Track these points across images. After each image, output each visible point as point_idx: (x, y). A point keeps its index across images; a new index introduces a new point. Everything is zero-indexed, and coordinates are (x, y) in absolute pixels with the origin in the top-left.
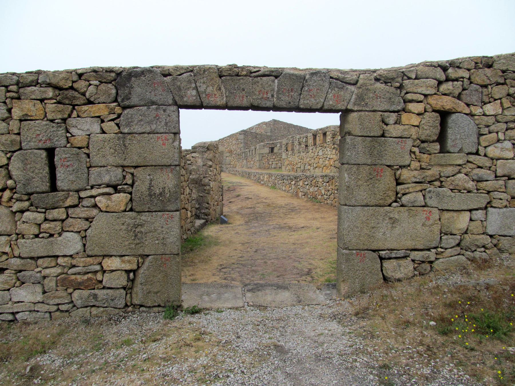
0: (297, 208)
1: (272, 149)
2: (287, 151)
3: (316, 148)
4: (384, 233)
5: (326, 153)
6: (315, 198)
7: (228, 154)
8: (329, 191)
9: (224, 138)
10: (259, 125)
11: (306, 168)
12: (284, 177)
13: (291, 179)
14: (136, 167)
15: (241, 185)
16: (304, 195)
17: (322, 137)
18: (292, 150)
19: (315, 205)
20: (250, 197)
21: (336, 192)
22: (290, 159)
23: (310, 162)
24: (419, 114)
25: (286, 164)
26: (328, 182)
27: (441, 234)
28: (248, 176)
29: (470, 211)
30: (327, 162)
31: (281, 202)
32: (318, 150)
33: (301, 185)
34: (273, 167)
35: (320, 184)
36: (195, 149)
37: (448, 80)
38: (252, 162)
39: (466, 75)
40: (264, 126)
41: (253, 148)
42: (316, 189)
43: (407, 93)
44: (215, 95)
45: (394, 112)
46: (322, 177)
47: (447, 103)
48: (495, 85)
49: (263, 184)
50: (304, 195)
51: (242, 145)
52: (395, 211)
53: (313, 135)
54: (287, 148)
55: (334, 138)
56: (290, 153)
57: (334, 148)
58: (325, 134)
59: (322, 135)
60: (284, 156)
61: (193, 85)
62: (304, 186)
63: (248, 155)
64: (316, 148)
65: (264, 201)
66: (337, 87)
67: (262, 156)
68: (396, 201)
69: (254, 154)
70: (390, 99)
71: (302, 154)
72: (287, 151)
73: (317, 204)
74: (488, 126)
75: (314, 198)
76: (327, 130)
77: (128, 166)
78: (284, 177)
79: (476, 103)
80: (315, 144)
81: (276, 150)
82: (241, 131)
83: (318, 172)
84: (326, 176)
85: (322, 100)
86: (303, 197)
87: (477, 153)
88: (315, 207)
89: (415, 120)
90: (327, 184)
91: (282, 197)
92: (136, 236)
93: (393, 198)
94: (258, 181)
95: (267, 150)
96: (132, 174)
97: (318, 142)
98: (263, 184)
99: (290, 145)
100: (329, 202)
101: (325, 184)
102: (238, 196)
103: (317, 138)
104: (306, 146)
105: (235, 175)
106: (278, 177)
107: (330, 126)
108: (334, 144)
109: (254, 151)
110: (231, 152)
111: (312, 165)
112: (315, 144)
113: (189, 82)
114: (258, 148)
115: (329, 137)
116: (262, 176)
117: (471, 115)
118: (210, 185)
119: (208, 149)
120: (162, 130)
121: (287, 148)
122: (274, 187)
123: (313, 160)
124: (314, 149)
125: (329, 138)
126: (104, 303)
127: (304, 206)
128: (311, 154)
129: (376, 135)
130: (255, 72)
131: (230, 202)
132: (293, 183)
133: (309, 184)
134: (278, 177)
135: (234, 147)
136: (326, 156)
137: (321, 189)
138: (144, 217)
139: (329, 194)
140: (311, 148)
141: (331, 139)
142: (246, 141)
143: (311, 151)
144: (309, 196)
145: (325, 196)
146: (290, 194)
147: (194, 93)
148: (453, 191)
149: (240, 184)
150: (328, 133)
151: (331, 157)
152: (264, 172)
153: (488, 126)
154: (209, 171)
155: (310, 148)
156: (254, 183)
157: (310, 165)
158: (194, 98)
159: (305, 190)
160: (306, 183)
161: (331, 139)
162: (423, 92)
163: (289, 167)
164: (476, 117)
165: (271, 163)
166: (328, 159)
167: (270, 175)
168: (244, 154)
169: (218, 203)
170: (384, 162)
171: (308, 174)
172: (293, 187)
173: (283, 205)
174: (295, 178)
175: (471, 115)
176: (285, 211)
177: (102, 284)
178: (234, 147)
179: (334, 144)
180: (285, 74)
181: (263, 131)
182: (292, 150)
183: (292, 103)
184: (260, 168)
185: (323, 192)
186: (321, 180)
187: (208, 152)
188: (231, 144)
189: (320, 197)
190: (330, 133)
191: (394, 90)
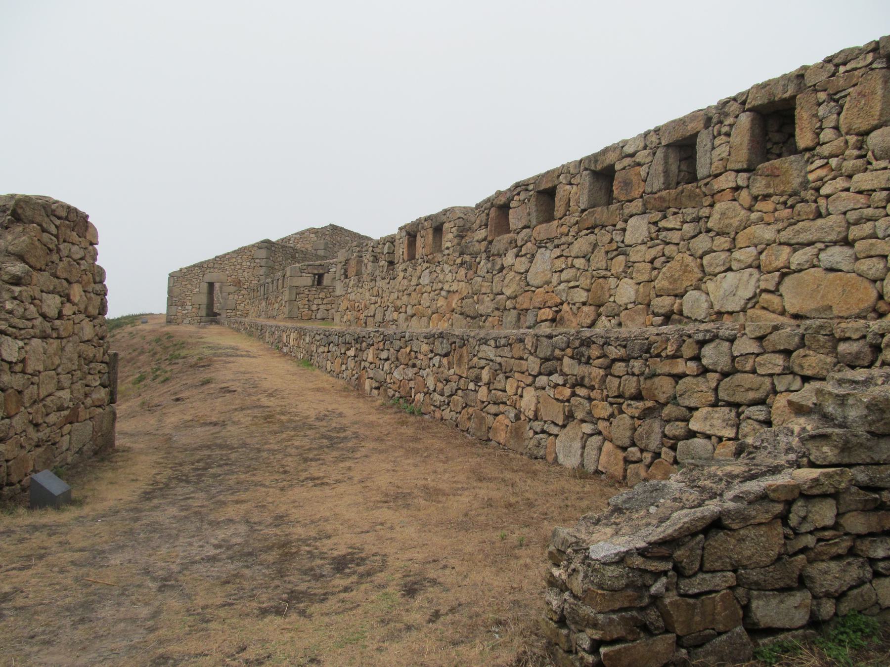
0: (348, 433)
1: (319, 279)
2: (346, 277)
3: (414, 267)
5: (441, 277)
6: (407, 398)
7: (232, 289)
8: (448, 381)
9: (225, 255)
10: (302, 233)
11: (387, 318)
12: (331, 338)
13: (345, 343)
15: (235, 353)
16: (378, 388)
17: (431, 237)
19: (403, 423)
20: (233, 388)
21: (472, 386)
22: (352, 296)
23: (399, 303)
25: (342, 307)
26: (446, 355)
28: (257, 332)
30: (441, 302)
31: (309, 406)
32: (418, 272)
33: (370, 358)
34: (318, 317)
35: (422, 360)
36: (203, 291)
38: (276, 306)
40: (312, 235)
41: (279, 274)
42: (410, 372)
46: (430, 338)
49: (285, 354)
50: (378, 388)
51: (262, 271)
54: (346, 271)
55: (462, 237)
56: (352, 282)
57: (462, 264)
58: (438, 230)
59: (430, 231)
62: (378, 362)
63: (271, 290)
64: (414, 267)
65: (265, 401)
67: (297, 291)
69: (280, 288)
71: (381, 283)
72: (346, 277)
73: (412, 419)
75: (402, 402)
76: (444, 218)
78: (331, 338)
80: (412, 257)
81: (326, 281)
82: (262, 242)
83: (417, 327)
84: (441, 335)
86: (375, 392)
88: (404, 429)
90: (445, 361)
91: (318, 390)
94: (278, 347)
95: (307, 280)
97: (420, 251)
98: (285, 354)
99: (353, 263)
100: (447, 414)
101: (436, 360)
102: (207, 382)
103: (419, 241)
104: (391, 263)
105: (238, 330)
106: (318, 337)
107: (453, 208)
108: (462, 253)
109: (280, 281)
110: (238, 283)
111: (403, 310)
112: (412, 257)
114: (288, 274)
115: (451, 236)
116: (284, 335)
119: (17, 217)
121: (346, 271)
122: (308, 361)
123: (405, 298)
124: (410, 270)
125: (449, 239)
127: (371, 425)
128: (401, 282)
131: (178, 400)
132: (351, 353)
133: (393, 358)
134: (318, 337)
135: (245, 274)
136: (440, 285)
137: (424, 373)
139: (447, 392)
141: (456, 241)
142: (271, 263)
143: (401, 274)
144: (391, 392)
145: (436, 397)
146: (341, 382)
149: (230, 351)
150: (446, 226)
151: (454, 287)
152: (289, 324)
154: (6, 296)
155: (400, 267)
156: (268, 350)
157: (397, 309)
159: (381, 375)
160: (384, 355)
161: (456, 241)
163: (349, 316)
165: (314, 307)
166: (443, 293)
167: (302, 333)
168: (262, 288)
171: (390, 330)
172: (351, 364)
173: (310, 421)
174: (356, 340)
176: (306, 443)
178: (245, 274)
179: (462, 253)
181: (309, 246)
184: (291, 318)
185: (431, 383)
186: (425, 348)
187: (19, 228)
188: (238, 267)
189: (420, 397)
190: (452, 224)
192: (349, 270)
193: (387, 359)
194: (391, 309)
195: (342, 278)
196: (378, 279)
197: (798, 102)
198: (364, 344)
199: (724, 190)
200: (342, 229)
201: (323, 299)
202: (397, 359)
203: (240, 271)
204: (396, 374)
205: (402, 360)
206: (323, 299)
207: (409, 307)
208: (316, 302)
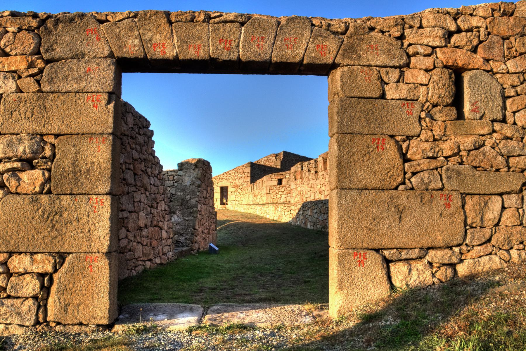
4: (390, 227)
14: (57, 136)
18: (301, 178)
23: (321, 190)
24: (427, 71)
27: (465, 227)
29: (501, 195)
37: (459, 31)
39: (481, 23)
43: (410, 45)
44: (163, 44)
45: (395, 67)
47: (461, 58)
48: (519, 35)
52: (402, 197)
53: (324, 159)
56: (298, 183)
60: (293, 186)
61: (136, 33)
66: (321, 36)
68: (403, 183)
70: (389, 50)
74: (514, 87)
77: (47, 134)
79: (497, 58)
80: (325, 169)
85: (302, 52)
87: (504, 120)
89: (423, 78)
92: (53, 226)
93: (400, 179)
95: (275, 182)
96: (53, 146)
113: (131, 29)
117: (491, 72)
118: (197, 208)
120: (93, 89)
126: (7, 319)
129: (374, 96)
130: (215, 17)
133: (318, 212)
138: (66, 200)
140: (322, 173)
143: (321, 177)
147: (136, 42)
148: (478, 169)
153: (514, 87)
155: (320, 174)
158: (137, 48)
162: (430, 44)
164: (498, 76)
165: (279, 196)
169: (209, 231)
170: (385, 131)
175: (491, 72)
177: (6, 292)
178: (240, 181)
180: (254, 19)
182: (301, 178)
183: (262, 55)
191: (394, 40)
192: (297, 176)
193: (316, 213)
194: (318, 193)
195: (294, 180)
196: (311, 179)
197: (117, 312)
198: (306, 208)
199: (70, 92)
200: (290, 153)
201: (283, 192)
202: (321, 212)
203: (237, 180)
204: (320, 218)
205: (322, 212)
206: (283, 192)
207: (326, 191)
208: (280, 193)
